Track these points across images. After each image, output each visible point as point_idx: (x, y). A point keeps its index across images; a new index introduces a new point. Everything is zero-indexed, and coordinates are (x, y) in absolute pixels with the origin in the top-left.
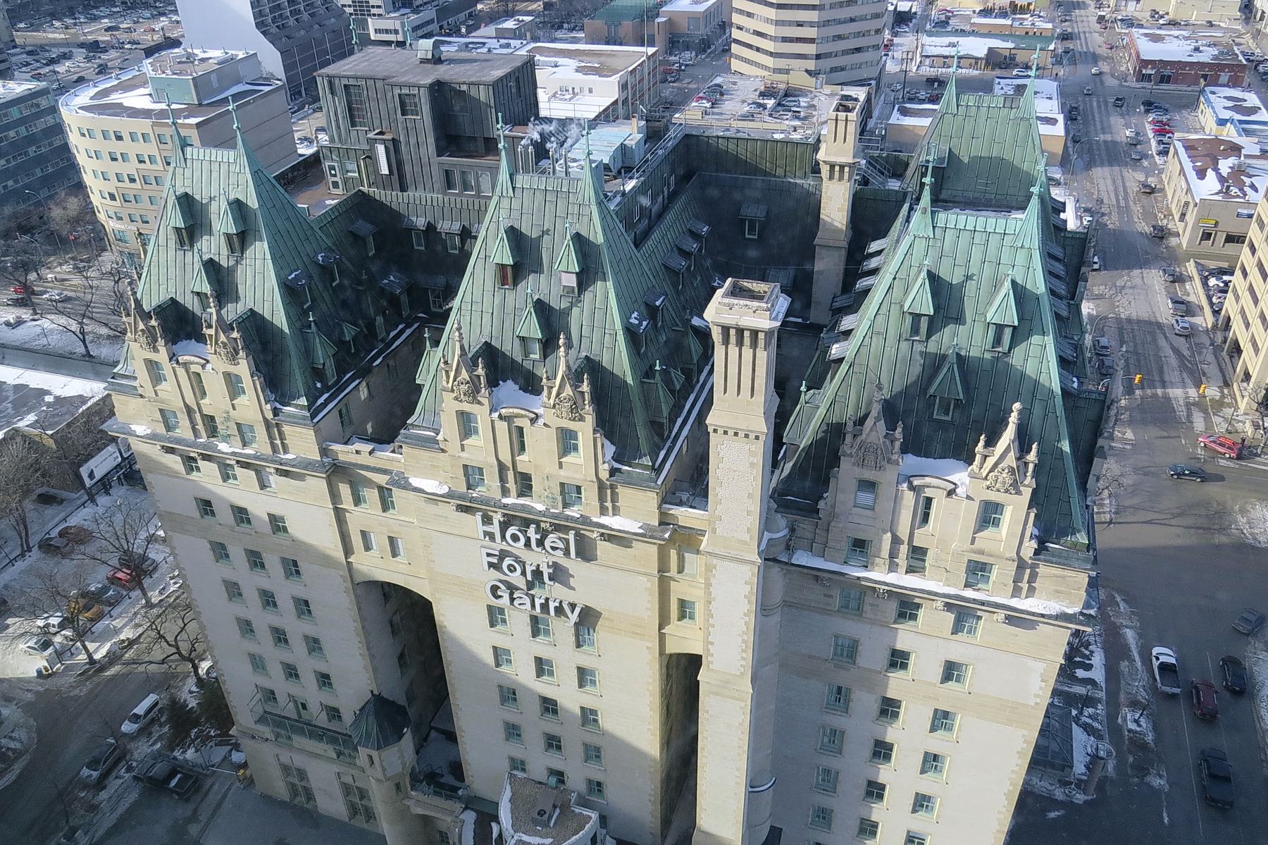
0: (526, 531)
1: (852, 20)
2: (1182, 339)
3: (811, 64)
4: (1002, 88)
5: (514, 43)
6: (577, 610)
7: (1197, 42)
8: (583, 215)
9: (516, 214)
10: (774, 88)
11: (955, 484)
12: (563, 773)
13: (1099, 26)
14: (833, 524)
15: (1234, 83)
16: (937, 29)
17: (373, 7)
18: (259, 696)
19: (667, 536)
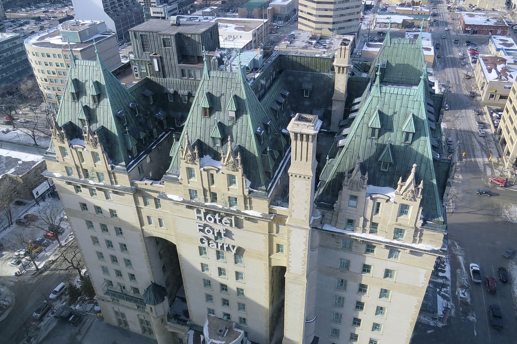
0: (214, 216)
1: (347, 8)
2: (482, 138)
3: (331, 26)
4: (409, 36)
5: (210, 17)
6: (235, 248)
7: (488, 17)
8: (238, 88)
9: (210, 87)
10: (316, 36)
11: (389, 197)
12: (229, 315)
13: (448, 10)
14: (339, 213)
15: (503, 34)
16: (382, 12)
17: (152, 3)
18: (106, 283)
19: (272, 218)
